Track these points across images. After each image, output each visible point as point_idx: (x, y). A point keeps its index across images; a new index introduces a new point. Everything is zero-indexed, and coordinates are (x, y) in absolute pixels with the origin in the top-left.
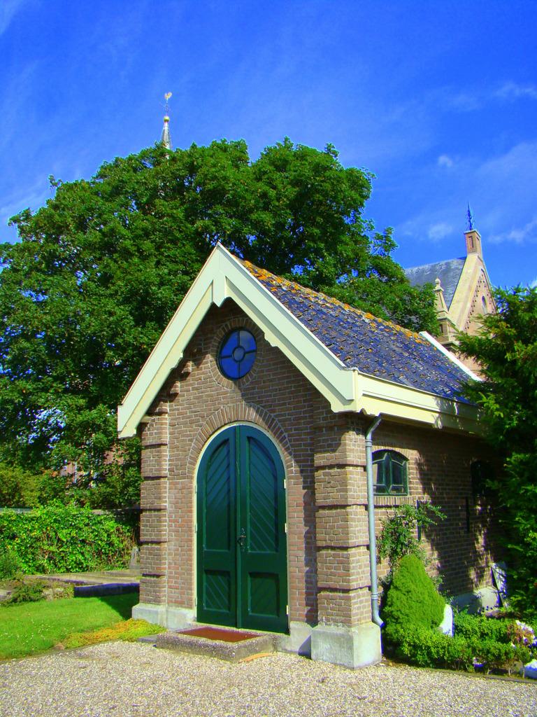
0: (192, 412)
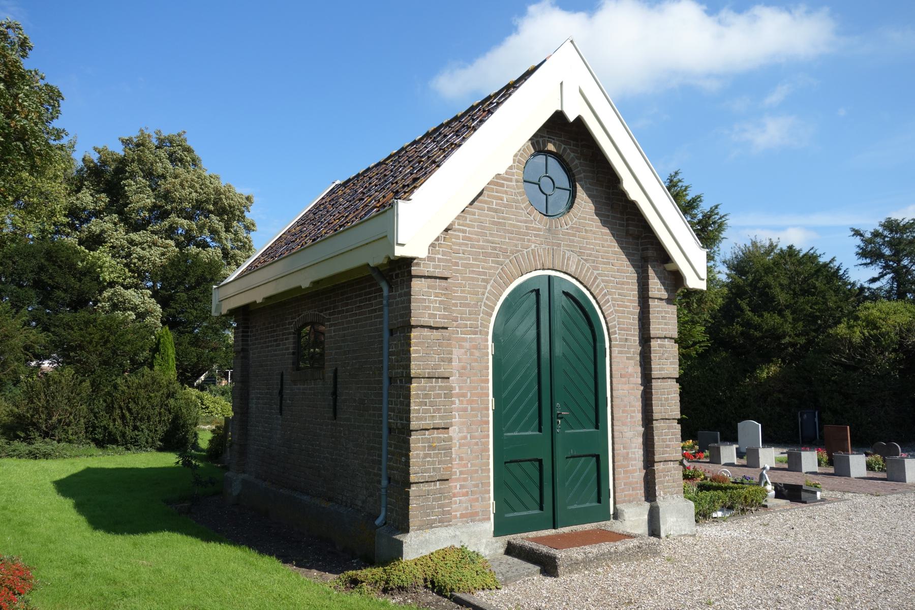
0: (488, 241)
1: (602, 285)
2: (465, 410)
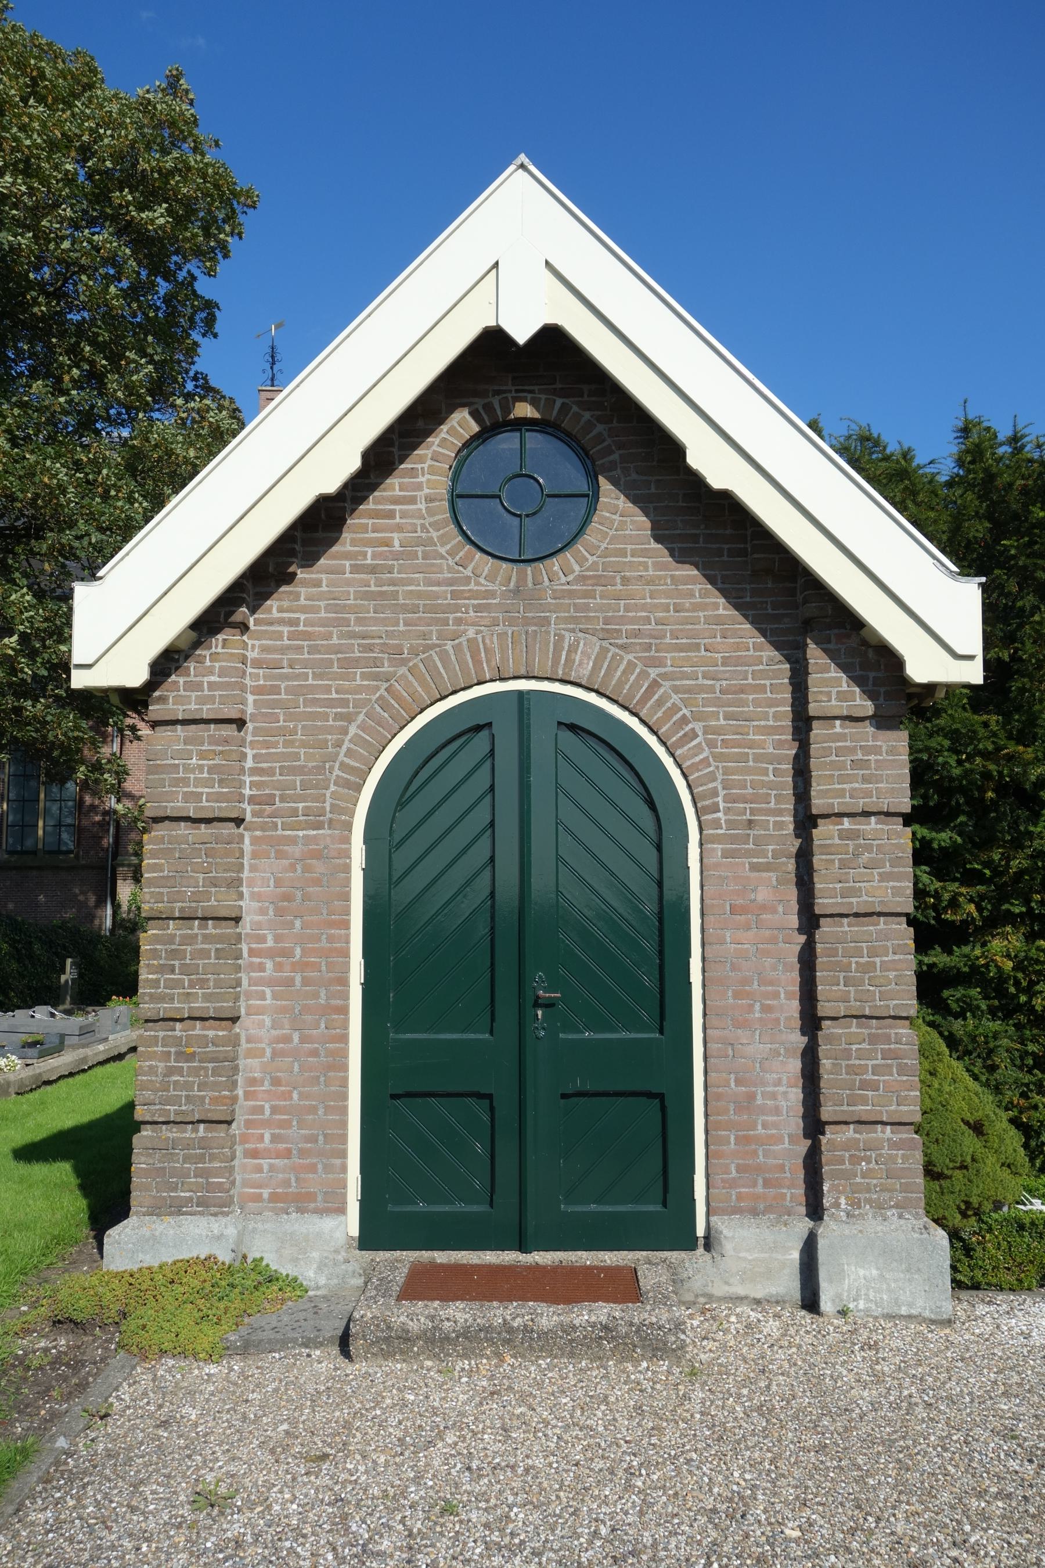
0: (352, 635)
1: (675, 698)
2: (289, 983)
